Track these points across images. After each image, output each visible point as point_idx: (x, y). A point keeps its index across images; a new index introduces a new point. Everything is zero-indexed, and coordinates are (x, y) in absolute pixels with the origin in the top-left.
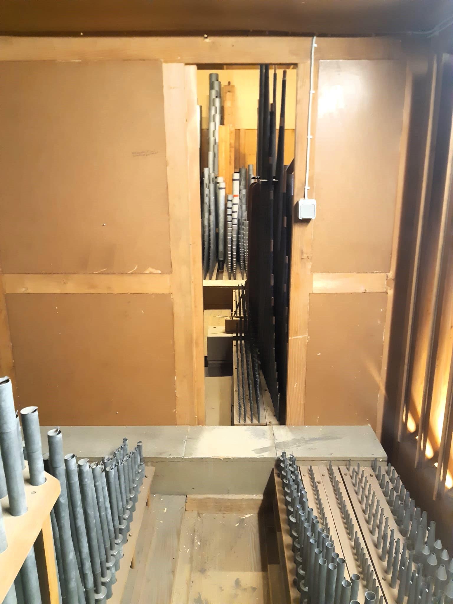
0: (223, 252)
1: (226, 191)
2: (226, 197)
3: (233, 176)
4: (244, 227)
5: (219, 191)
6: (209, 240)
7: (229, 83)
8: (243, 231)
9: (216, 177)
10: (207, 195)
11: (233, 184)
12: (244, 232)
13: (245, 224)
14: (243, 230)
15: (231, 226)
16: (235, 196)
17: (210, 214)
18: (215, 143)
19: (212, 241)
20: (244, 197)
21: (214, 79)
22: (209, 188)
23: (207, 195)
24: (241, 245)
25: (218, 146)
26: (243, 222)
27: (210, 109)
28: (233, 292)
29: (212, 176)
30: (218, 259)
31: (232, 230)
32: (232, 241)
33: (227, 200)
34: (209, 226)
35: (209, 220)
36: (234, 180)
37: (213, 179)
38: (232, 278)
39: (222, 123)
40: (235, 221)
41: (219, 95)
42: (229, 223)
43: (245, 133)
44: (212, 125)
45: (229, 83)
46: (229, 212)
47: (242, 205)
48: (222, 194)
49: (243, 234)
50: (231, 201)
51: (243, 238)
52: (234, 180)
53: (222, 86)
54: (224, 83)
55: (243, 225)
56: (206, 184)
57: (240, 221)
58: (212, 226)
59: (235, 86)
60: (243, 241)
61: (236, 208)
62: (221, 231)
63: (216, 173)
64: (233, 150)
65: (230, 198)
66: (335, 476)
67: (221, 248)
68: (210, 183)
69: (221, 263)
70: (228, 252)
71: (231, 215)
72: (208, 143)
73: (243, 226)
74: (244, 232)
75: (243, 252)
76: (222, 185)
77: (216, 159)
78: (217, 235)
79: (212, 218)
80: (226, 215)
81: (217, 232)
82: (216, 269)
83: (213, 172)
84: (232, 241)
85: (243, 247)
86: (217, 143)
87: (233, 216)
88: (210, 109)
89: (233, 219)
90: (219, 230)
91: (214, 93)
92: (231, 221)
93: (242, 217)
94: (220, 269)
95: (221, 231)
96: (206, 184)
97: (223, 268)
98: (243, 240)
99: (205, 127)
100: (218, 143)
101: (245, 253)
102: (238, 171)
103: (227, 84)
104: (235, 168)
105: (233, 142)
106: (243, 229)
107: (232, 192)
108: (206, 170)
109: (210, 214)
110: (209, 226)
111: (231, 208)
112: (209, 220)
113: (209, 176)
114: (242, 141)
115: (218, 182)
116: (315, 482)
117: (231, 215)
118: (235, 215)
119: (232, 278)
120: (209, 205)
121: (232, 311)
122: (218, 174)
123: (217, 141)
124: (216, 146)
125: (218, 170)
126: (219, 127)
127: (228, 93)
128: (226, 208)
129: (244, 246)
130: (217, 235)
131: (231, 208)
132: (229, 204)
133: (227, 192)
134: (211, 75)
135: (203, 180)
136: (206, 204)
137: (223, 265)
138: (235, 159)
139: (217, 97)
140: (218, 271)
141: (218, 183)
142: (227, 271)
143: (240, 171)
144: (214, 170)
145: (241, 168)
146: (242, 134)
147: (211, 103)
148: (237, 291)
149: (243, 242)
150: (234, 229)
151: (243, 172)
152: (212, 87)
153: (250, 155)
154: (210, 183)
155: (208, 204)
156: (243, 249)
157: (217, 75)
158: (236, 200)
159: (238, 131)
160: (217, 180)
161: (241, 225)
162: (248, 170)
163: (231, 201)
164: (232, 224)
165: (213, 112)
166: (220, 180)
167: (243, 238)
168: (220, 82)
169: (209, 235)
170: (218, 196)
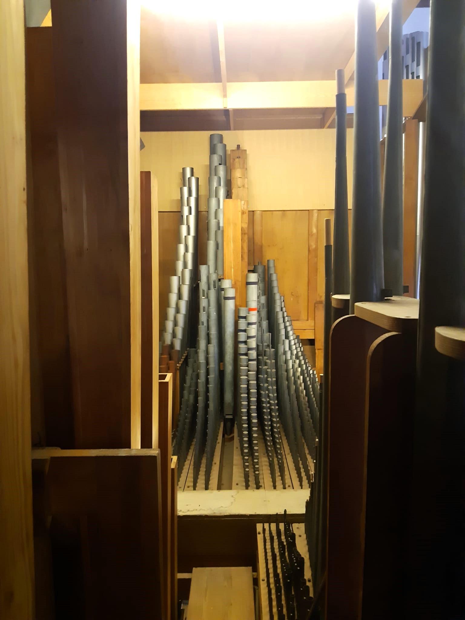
0: (232, 404)
1: (235, 302)
2: (237, 311)
3: (247, 277)
4: (267, 359)
5: (224, 303)
6: (207, 390)
7: (238, 146)
8: (266, 367)
9: (220, 280)
10: (204, 308)
11: (247, 289)
12: (268, 369)
13: (268, 353)
14: (266, 365)
15: (245, 364)
16: (250, 310)
17: (209, 342)
18: (219, 228)
19: (212, 394)
20: (263, 308)
21: (216, 141)
22: (208, 297)
23: (204, 308)
24: (263, 396)
25: (223, 231)
26: (265, 351)
27: (210, 181)
28: (258, 535)
29: (214, 277)
30: (224, 417)
31: (249, 371)
32: (248, 393)
33: (238, 317)
34: (207, 363)
35: (207, 352)
36: (248, 283)
37: (214, 282)
38: (252, 483)
39: (229, 195)
40: (253, 354)
41: (224, 161)
42: (242, 357)
43: (262, 216)
44: (213, 201)
45: (238, 146)
46: (242, 336)
47: (261, 320)
48: (230, 306)
49: (267, 373)
50: (245, 318)
51: (267, 382)
52: (248, 283)
53: (229, 152)
54: (231, 146)
55: (265, 355)
56: (203, 291)
57: (261, 348)
58: (213, 365)
59: (247, 152)
60: (268, 386)
61: (253, 331)
62: (229, 368)
63: (220, 273)
64: (246, 237)
65: (242, 314)
66: (223, 108)
67: (228, 397)
68: (209, 289)
69: (229, 424)
70: (242, 402)
71: (245, 343)
72: (208, 229)
73: (265, 358)
74: (268, 369)
75: (269, 410)
76: (231, 293)
77: (220, 252)
78: (221, 374)
79: (213, 348)
80: (236, 342)
81: (221, 369)
82: (219, 443)
83: (215, 272)
84: (248, 393)
85: (268, 400)
86: (221, 229)
87: (248, 343)
88: (210, 181)
89: (249, 337)
90: (224, 365)
91: (216, 158)
92: (246, 354)
93: (262, 343)
94: (227, 434)
95: (229, 368)
96: (203, 291)
97: (232, 432)
98: (266, 385)
99: (202, 208)
100: (223, 227)
101: (273, 414)
102: (252, 268)
103: (235, 148)
104: (249, 264)
105: (245, 226)
106: (266, 364)
107: (246, 304)
108: (203, 269)
109: (209, 342)
110: (207, 363)
111: (245, 331)
112: (207, 352)
113: (208, 278)
114: (258, 228)
115: (223, 287)
116: (265, 295)
117: (245, 343)
118: (253, 343)
119: (252, 483)
120: (207, 327)
121: (255, 569)
122: (223, 275)
123: (221, 225)
124: (219, 232)
125: (223, 267)
126: (224, 201)
127: (237, 160)
128: (237, 330)
129: (269, 397)
130: (221, 374)
131: (245, 331)
132: (242, 324)
133: (238, 304)
134: (211, 136)
135: (199, 284)
136: (203, 324)
137: (233, 426)
138: (249, 251)
139: (220, 164)
140: (223, 436)
141: (223, 289)
142: (239, 448)
143: (254, 268)
144: (216, 268)
145: (257, 264)
146: (257, 216)
147: (212, 171)
148: (266, 526)
149: (268, 389)
150: (251, 369)
151: (260, 269)
152: (213, 151)
153: (269, 246)
154: (209, 289)
155: (205, 324)
156: (268, 405)
157: (221, 136)
158: (253, 317)
159: (252, 213)
160: (221, 283)
161: (261, 355)
162: (266, 268)
163: (245, 318)
164: (247, 361)
165: (215, 184)
166: (226, 284)
167: (267, 382)
168: (225, 145)
169: (207, 381)
170: (223, 309)
